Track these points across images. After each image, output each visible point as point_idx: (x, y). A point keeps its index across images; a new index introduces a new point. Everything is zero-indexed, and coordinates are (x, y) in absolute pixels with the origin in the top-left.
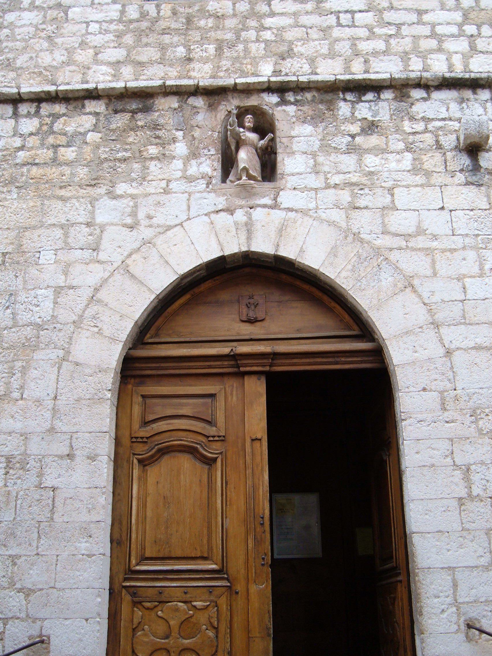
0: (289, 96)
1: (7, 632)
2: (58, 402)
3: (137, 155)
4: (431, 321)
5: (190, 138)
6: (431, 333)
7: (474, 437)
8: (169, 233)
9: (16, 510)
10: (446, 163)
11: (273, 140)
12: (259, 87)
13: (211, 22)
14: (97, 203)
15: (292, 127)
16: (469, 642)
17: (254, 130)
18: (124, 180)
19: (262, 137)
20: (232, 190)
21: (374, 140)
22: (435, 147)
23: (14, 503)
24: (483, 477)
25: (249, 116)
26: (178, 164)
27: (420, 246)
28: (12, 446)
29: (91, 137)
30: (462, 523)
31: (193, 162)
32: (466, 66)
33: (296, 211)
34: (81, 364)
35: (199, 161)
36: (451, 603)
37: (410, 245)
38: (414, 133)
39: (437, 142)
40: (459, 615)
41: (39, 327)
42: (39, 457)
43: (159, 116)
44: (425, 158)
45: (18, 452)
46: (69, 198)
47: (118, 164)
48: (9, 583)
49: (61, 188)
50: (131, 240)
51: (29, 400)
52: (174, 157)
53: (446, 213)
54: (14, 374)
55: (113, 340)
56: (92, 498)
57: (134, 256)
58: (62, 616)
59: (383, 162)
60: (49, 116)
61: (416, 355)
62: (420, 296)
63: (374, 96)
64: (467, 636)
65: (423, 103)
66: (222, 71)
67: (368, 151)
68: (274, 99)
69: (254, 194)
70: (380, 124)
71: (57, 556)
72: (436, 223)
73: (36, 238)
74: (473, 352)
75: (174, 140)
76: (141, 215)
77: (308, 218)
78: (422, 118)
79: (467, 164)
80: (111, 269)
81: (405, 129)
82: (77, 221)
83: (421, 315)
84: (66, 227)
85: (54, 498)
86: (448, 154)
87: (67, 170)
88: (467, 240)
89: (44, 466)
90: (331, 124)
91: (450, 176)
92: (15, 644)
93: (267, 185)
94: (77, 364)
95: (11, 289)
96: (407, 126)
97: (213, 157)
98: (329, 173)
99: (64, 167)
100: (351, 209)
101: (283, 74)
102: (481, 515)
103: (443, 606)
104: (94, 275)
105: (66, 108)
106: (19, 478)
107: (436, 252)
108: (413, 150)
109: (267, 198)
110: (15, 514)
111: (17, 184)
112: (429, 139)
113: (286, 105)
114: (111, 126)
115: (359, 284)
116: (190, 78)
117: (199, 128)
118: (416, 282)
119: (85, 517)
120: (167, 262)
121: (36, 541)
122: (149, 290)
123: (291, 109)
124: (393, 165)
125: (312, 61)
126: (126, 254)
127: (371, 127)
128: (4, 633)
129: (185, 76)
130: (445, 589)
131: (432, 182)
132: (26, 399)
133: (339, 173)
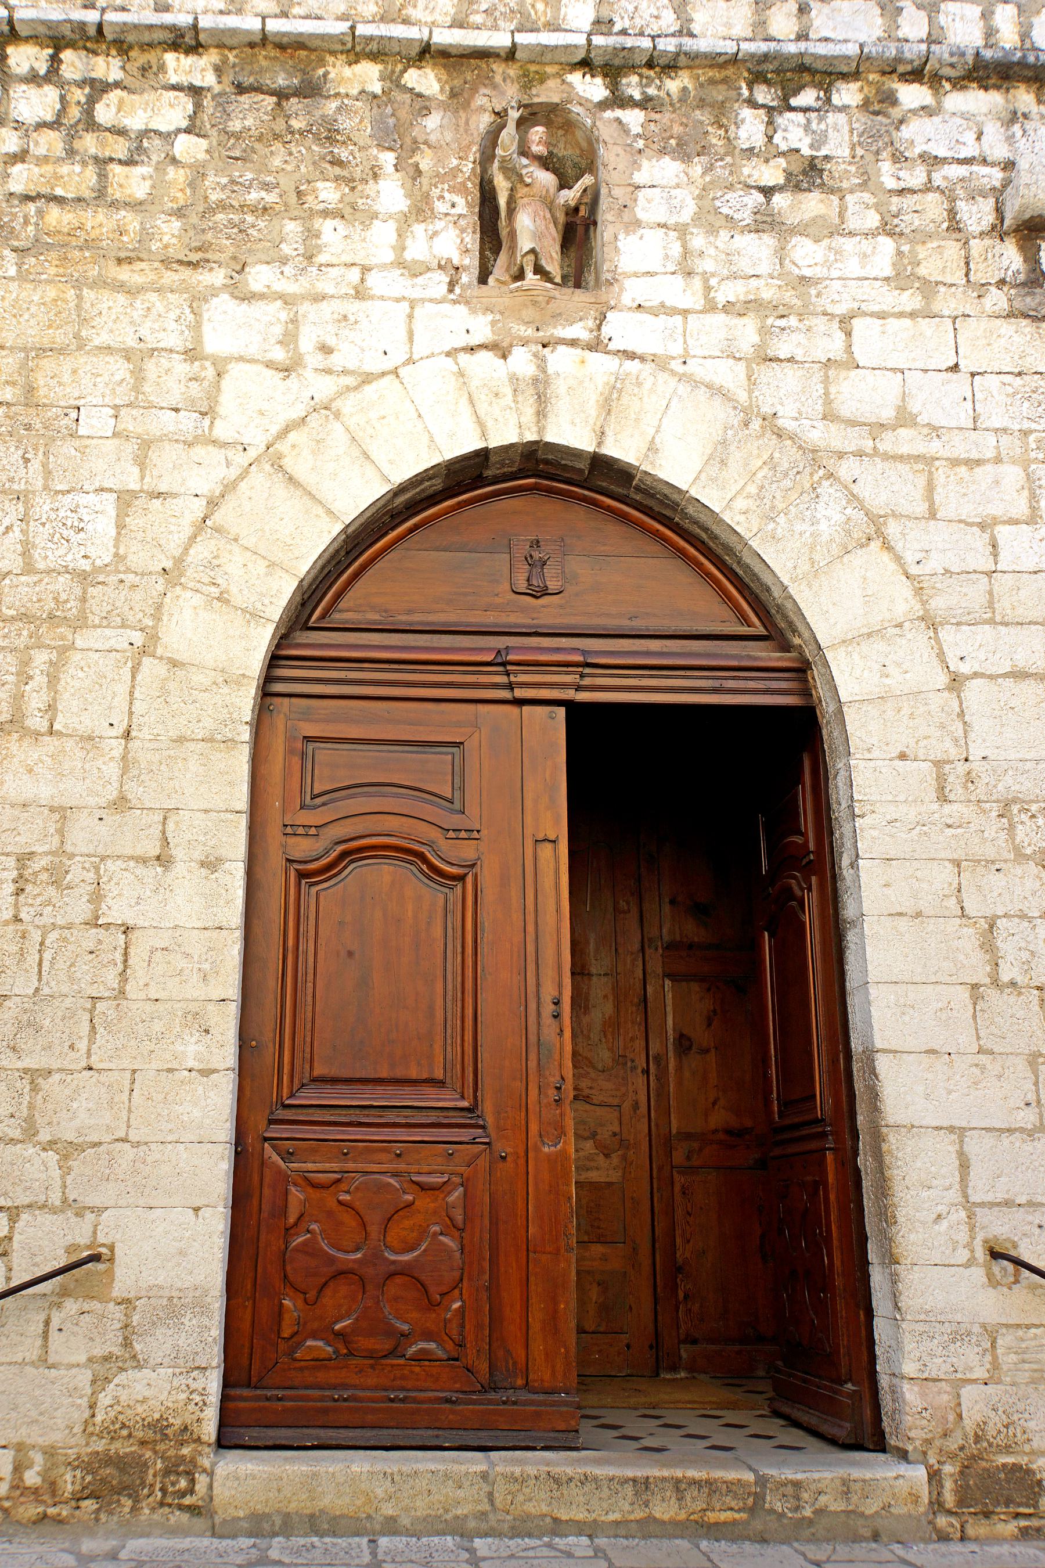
0: (628, 85)
1: (17, 1238)
2: (133, 745)
3: (293, 199)
4: (921, 613)
5: (411, 171)
6: (919, 639)
7: (1006, 861)
8: (367, 388)
9: (40, 972)
10: (967, 264)
11: (593, 198)
12: (461, 51)
14: (205, 307)
15: (635, 162)
16: (995, 1288)
17: (546, 162)
18: (264, 258)
19: (564, 184)
20: (506, 301)
21: (813, 204)
22: (945, 225)
23: (37, 957)
24: (1023, 945)
25: (540, 129)
26: (384, 233)
27: (905, 450)
28: (34, 835)
29: (187, 147)
30: (978, 1038)
31: (419, 229)
32: (1025, 35)
33: (642, 359)
34: (184, 664)
35: (431, 227)
36: (956, 1201)
37: (882, 447)
38: (901, 192)
39: (952, 213)
40: (972, 1229)
41: (83, 577)
42: (93, 859)
43: (339, 109)
44: (922, 252)
45: (46, 848)
46: (141, 290)
47: (250, 219)
48: (24, 1131)
49: (119, 261)
50: (287, 399)
51: (67, 735)
52: (375, 216)
53: (961, 380)
54: (31, 678)
55: (254, 616)
56: (210, 949)
57: (292, 436)
58: (141, 1203)
60: (81, 84)
61: (887, 681)
62: (898, 559)
63: (818, 98)
64: (990, 1276)
65: (927, 119)
66: (478, 12)
67: (801, 230)
70: (829, 166)
71: (134, 1071)
72: (940, 401)
73: (66, 378)
74: (1009, 682)
76: (306, 344)
77: (666, 375)
78: (921, 156)
79: (1014, 267)
80: (241, 460)
81: (882, 179)
82: (161, 345)
83: (901, 601)
84: (137, 357)
85: (126, 948)
86: (972, 242)
87: (132, 221)
89: (104, 879)
90: (722, 160)
91: (975, 294)
92: (35, 1265)
94: (174, 664)
95: (16, 487)
96: (887, 174)
97: (462, 222)
98: (713, 275)
99: (123, 213)
100: (758, 360)
101: (617, 28)
102: (1018, 1018)
103: (940, 1207)
104: (205, 472)
105: (123, 68)
106: (49, 903)
107: (937, 463)
108: (898, 230)
109: (581, 324)
110: (40, 980)
111: (16, 243)
112: (934, 206)
114: (230, 123)
115: (772, 526)
116: (406, 21)
117: (429, 147)
118: (892, 529)
119: (195, 990)
120: (367, 457)
121: (85, 1041)
122: (330, 512)
123: (633, 118)
124: (853, 267)
126: (275, 429)
127: (808, 174)
128: (11, 1239)
129: (395, 16)
130: (944, 1171)
131: (936, 307)
132: (60, 734)
133: (734, 276)
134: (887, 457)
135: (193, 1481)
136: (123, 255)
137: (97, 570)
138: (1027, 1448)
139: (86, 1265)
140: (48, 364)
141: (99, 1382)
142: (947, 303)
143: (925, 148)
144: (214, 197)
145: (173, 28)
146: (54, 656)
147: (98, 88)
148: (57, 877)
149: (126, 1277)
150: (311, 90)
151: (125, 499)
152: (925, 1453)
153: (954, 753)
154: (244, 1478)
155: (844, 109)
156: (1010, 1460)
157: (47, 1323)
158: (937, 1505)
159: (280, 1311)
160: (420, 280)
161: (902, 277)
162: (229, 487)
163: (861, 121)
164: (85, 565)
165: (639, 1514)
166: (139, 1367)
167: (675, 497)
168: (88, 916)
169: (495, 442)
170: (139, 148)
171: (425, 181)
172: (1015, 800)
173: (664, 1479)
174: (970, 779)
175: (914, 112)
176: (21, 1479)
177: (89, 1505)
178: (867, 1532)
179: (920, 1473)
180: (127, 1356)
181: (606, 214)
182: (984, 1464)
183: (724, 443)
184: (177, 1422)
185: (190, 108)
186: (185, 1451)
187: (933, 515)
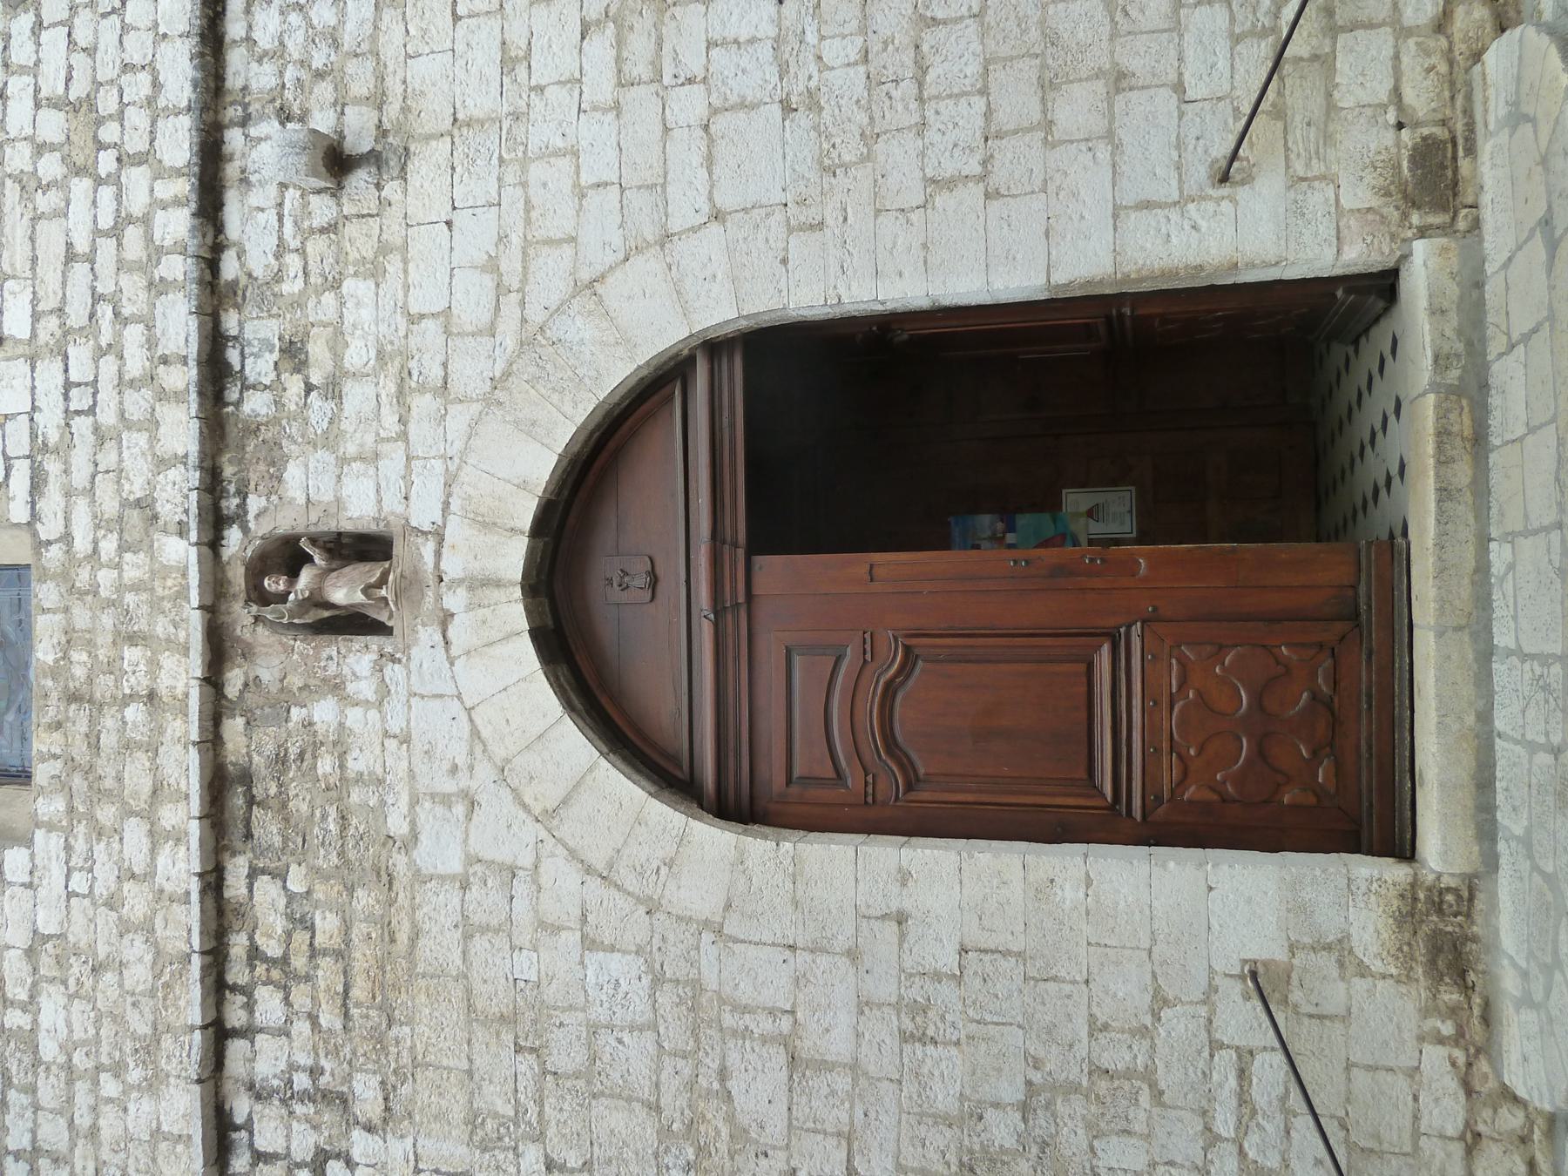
1: (1237, 1042)
6: (680, 247)
11: (313, 541)
13: (79, 656)
19: (308, 559)
21: (317, 350)
25: (266, 582)
26: (354, 716)
29: (296, 884)
31: (351, 688)
32: (178, 173)
39: (323, 231)
40: (1203, 198)
41: (658, 981)
43: (259, 754)
45: (894, 1018)
46: (414, 925)
48: (1143, 1037)
49: (393, 941)
50: (496, 805)
54: (747, 1028)
59: (358, 332)
60: (253, 968)
61: (719, 276)
64: (1243, 183)
66: (176, 635)
67: (337, 358)
69: (416, 572)
72: (476, 236)
74: (717, 170)
75: (308, 724)
76: (449, 786)
80: (550, 842)
83: (647, 266)
84: (468, 930)
88: (509, 178)
95: (584, 1035)
98: (378, 434)
104: (562, 878)
106: (943, 1018)
107: (529, 237)
112: (316, 246)
113: (246, 513)
116: (187, 695)
118: (585, 275)
120: (540, 737)
121: (1063, 986)
122: (590, 770)
123: (254, 503)
124: (366, 314)
125: (162, 464)
126: (522, 815)
127: (293, 353)
130: (1154, 224)
131: (399, 242)
134: (524, 280)
135: (1448, 889)
136: (387, 939)
137: (650, 969)
138: (1394, 150)
139: (1261, 983)
140: (480, 1004)
141: (1363, 971)
142: (394, 234)
143: (270, 256)
144: (335, 860)
145: (203, 892)
146: (728, 1008)
147: (254, 954)
148: (919, 1009)
149: (1267, 947)
150: (246, 778)
151: (590, 944)
152: (1404, 240)
153: (779, 216)
154: (1440, 842)
155: (241, 324)
156: (1405, 164)
157: (1311, 1016)
158: (1447, 230)
159: (1294, 807)
161: (375, 272)
162: (573, 854)
163: (250, 310)
164: (646, 980)
165: (1468, 498)
166: (1349, 936)
167: (565, 463)
168: (953, 984)
169: (523, 624)
170: (302, 920)
171: (312, 682)
172: (821, 163)
173: (1437, 475)
174: (802, 202)
175: (242, 265)
176: (1449, 1038)
177: (1471, 977)
178: (1475, 294)
179: (1419, 247)
180: (1341, 949)
181: (332, 525)
182: (1410, 188)
183: (517, 423)
184: (1396, 903)
185: (266, 878)
186: (1421, 896)
187: (573, 239)
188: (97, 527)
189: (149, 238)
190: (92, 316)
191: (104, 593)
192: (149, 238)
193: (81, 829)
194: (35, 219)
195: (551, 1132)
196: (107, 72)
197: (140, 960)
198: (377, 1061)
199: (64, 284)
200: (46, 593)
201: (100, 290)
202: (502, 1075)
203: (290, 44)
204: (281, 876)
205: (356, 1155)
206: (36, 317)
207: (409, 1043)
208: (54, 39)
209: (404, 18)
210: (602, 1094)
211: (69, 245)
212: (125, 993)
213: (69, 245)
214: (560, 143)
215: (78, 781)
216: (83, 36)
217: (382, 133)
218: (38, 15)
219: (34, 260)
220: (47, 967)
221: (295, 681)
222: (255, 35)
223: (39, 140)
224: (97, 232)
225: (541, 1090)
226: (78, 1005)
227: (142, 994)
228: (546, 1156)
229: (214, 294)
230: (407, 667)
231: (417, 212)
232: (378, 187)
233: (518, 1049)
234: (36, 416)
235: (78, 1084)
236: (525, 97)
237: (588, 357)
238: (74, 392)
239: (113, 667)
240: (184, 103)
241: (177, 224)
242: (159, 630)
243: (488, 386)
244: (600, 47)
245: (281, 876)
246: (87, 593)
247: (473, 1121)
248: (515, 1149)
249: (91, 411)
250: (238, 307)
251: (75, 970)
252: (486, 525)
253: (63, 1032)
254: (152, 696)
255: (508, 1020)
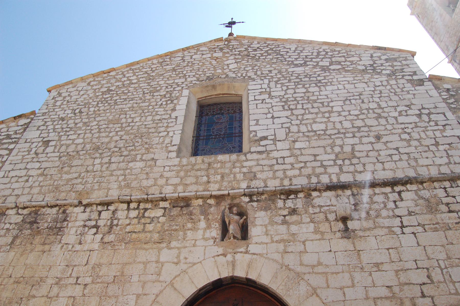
11: (246, 220)
13: (219, 165)
21: (295, 218)
26: (200, 232)
29: (162, 219)
31: (208, 231)
32: (338, 179)
39: (326, 217)
50: (175, 270)
60: (143, 209)
67: (292, 223)
68: (247, 199)
72: (327, 259)
76: (182, 258)
84: (145, 264)
93: (243, 242)
112: (322, 216)
113: (253, 202)
118: (319, 291)
120: (193, 282)
122: (183, 296)
123: (255, 204)
124: (305, 230)
125: (265, 181)
126: (173, 278)
127: (293, 212)
131: (325, 237)
134: (316, 273)
142: (327, 236)
144: (166, 228)
145: (161, 197)
147: (146, 210)
151: (138, 296)
155: (300, 198)
160: (207, 242)
161: (316, 231)
163: (304, 200)
171: (210, 221)
175: (316, 197)
183: (276, 273)
185: (163, 211)
187: (328, 287)
188: (250, 167)
189: (321, 174)
190: (301, 162)
191: (234, 170)
192: (321, 174)
193: (179, 168)
194: (324, 147)
195: (94, 285)
196: (362, 160)
197: (148, 183)
198: (117, 240)
199: (309, 155)
200: (234, 157)
201: (307, 163)
202: (109, 273)
203: (375, 204)
204: (164, 215)
205: (97, 236)
206: (300, 149)
207: (120, 248)
208: (369, 147)
209: (386, 235)
210: (101, 299)
211: (318, 155)
212: (141, 180)
213: (318, 155)
214: (355, 282)
215: (190, 167)
216: (371, 154)
217: (354, 231)
218: (375, 143)
219: (314, 148)
220: (149, 163)
221: (210, 217)
222: (376, 196)
223: (343, 146)
224: (322, 161)
225: (104, 283)
226: (140, 170)
227: (140, 184)
228: (88, 284)
229: (308, 192)
230: (212, 245)
231: (333, 242)
232: (339, 231)
233: (115, 277)
234: (276, 151)
235: (123, 171)
236: (368, 270)
237: (295, 293)
238: (282, 159)
239: (216, 173)
240: (356, 179)
241: (325, 180)
242: (224, 183)
243: (286, 264)
244: (384, 292)
245: (164, 215)
246: (234, 166)
247: (100, 265)
248: (91, 276)
249: (278, 163)
250: (305, 197)
251: (148, 169)
252: (249, 266)
253: (134, 167)
254: (209, 182)
255: (122, 274)
